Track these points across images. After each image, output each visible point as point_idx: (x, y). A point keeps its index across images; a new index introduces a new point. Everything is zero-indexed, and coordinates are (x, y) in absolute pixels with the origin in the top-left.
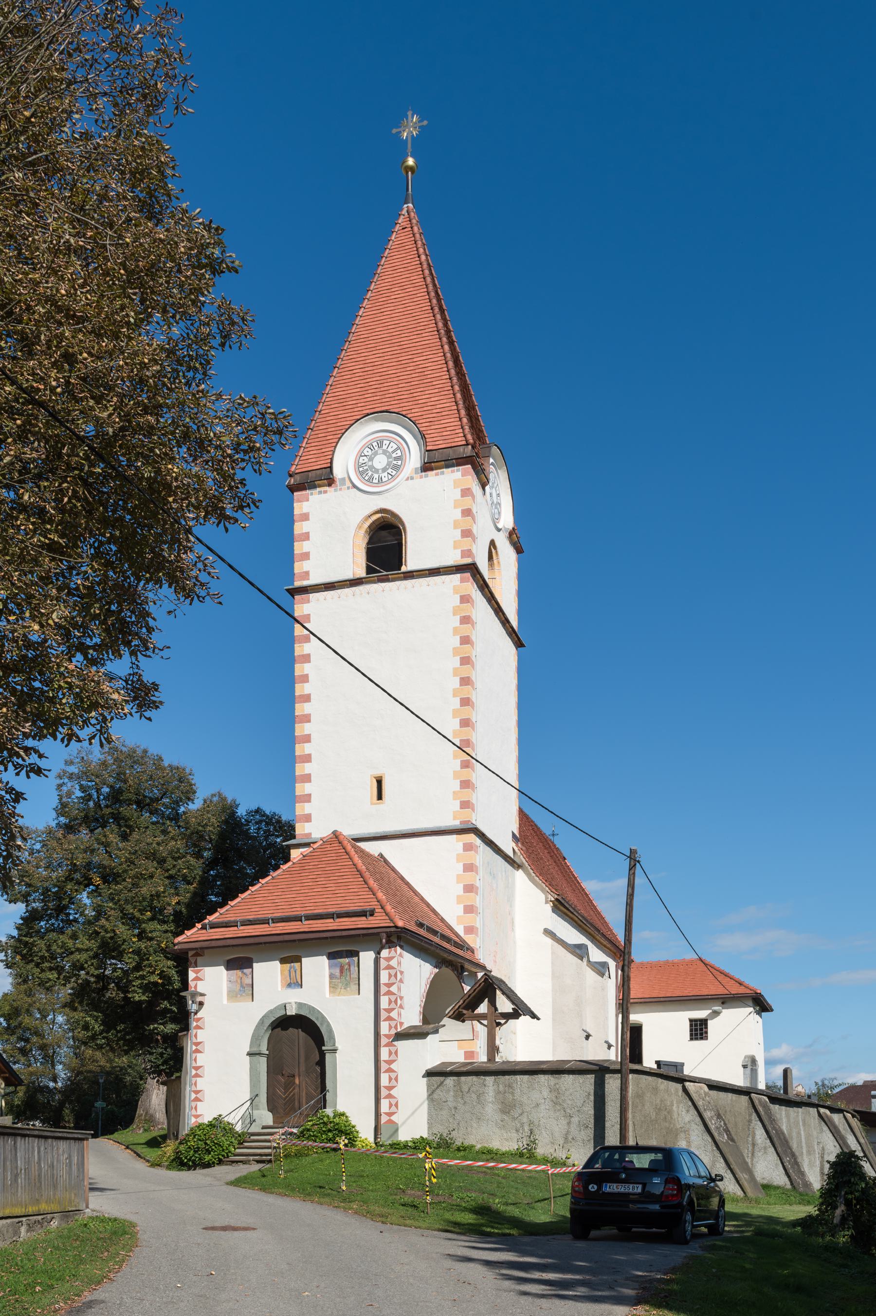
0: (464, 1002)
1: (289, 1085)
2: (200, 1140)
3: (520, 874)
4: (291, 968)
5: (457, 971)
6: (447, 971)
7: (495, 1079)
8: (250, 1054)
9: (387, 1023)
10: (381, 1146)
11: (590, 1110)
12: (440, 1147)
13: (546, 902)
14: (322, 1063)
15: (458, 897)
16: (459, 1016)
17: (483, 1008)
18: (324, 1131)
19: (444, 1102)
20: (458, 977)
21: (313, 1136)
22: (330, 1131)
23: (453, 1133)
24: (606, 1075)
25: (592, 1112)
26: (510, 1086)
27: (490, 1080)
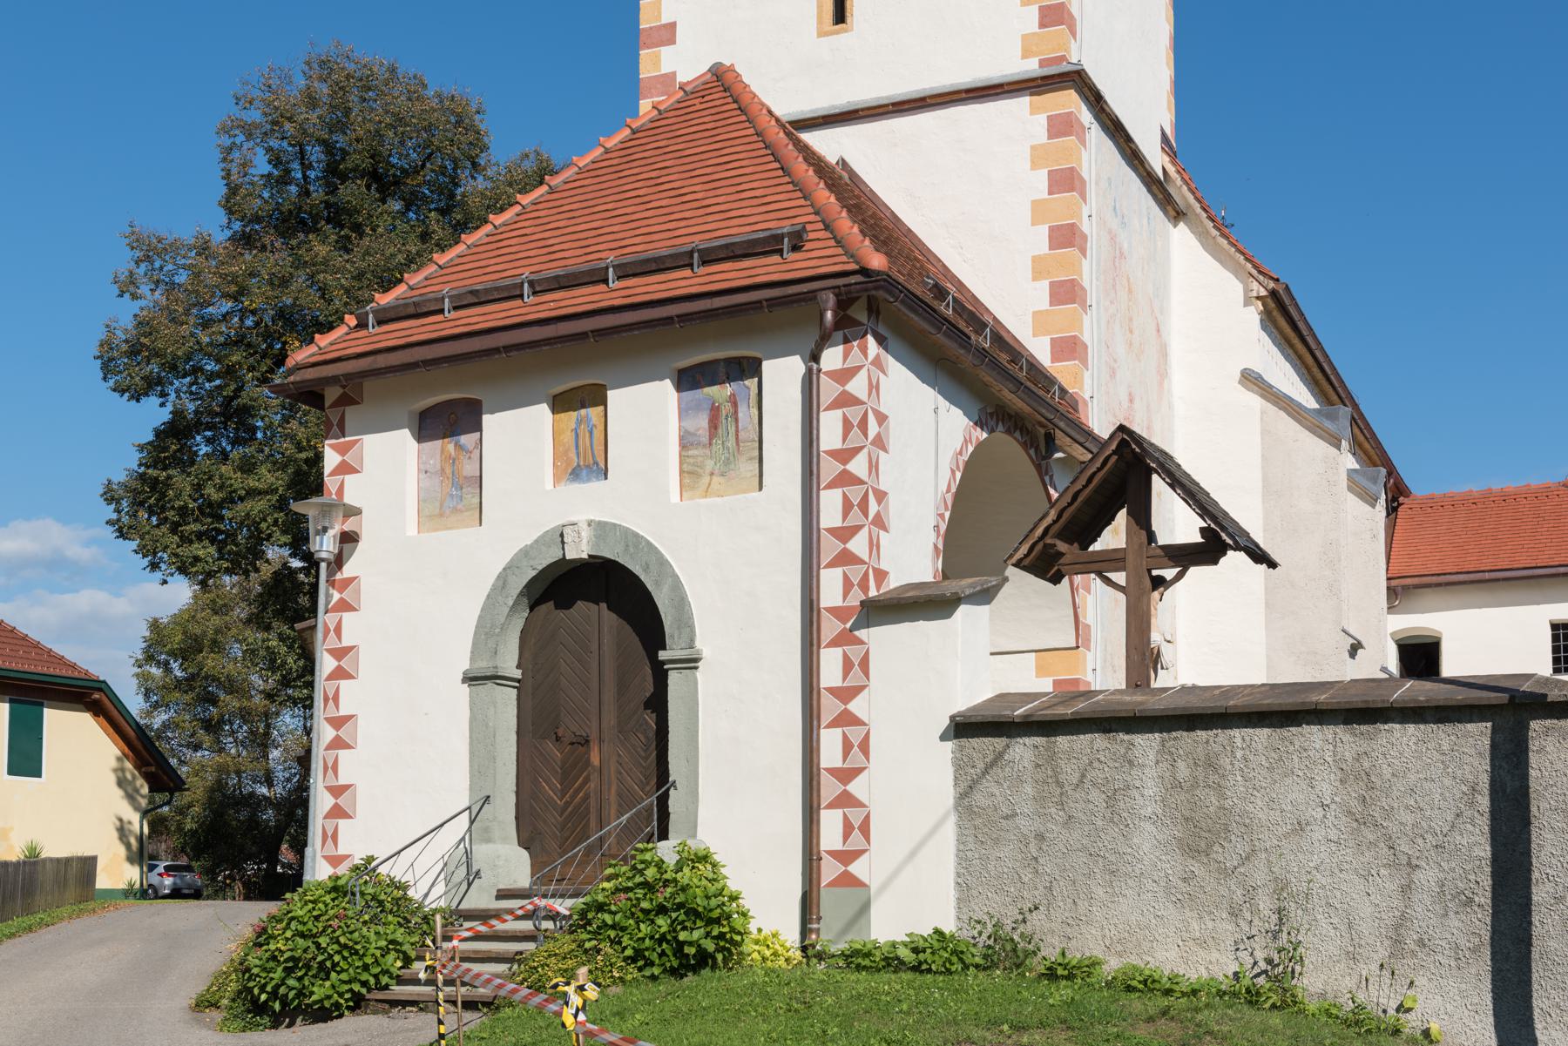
0: (1060, 516)
1: (574, 769)
2: (303, 935)
3: (1181, 236)
4: (579, 422)
5: (1037, 449)
6: (1010, 447)
7: (1163, 742)
8: (471, 679)
9: (838, 572)
10: (820, 956)
11: (1477, 842)
12: (994, 965)
13: (1247, 303)
14: (658, 703)
15: (1036, 205)
16: (1046, 566)
17: (1114, 536)
18: (646, 912)
19: (1007, 818)
20: (1038, 467)
21: (613, 927)
22: (662, 910)
23: (1036, 919)
24: (1535, 725)
25: (1484, 851)
26: (1211, 764)
27: (1146, 744)
